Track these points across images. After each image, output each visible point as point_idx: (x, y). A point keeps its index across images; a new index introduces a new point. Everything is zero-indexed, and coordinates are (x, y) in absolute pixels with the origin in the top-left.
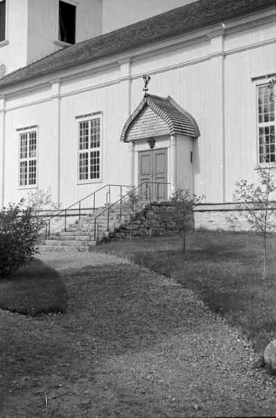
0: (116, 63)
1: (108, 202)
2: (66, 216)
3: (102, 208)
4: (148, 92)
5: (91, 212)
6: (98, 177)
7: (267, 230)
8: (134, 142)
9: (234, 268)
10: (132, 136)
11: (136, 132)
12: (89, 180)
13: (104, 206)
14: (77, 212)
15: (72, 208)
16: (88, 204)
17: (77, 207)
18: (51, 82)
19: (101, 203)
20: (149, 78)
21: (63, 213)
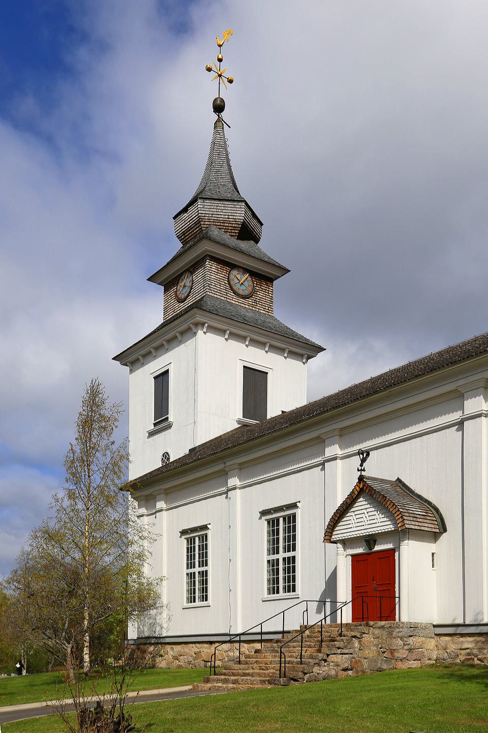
0: (318, 437)
1: (306, 624)
2: (240, 641)
3: (296, 631)
4: (363, 473)
5: (279, 636)
6: (294, 591)
7: (331, 685)
8: (345, 543)
9: (304, 361)
10: (338, 534)
11: (343, 531)
12: (282, 594)
13: (16, 558)
14: (258, 637)
15: (250, 631)
16: (274, 626)
17: (258, 630)
18: (227, 469)
19: (293, 625)
20: (368, 454)
21: (237, 638)
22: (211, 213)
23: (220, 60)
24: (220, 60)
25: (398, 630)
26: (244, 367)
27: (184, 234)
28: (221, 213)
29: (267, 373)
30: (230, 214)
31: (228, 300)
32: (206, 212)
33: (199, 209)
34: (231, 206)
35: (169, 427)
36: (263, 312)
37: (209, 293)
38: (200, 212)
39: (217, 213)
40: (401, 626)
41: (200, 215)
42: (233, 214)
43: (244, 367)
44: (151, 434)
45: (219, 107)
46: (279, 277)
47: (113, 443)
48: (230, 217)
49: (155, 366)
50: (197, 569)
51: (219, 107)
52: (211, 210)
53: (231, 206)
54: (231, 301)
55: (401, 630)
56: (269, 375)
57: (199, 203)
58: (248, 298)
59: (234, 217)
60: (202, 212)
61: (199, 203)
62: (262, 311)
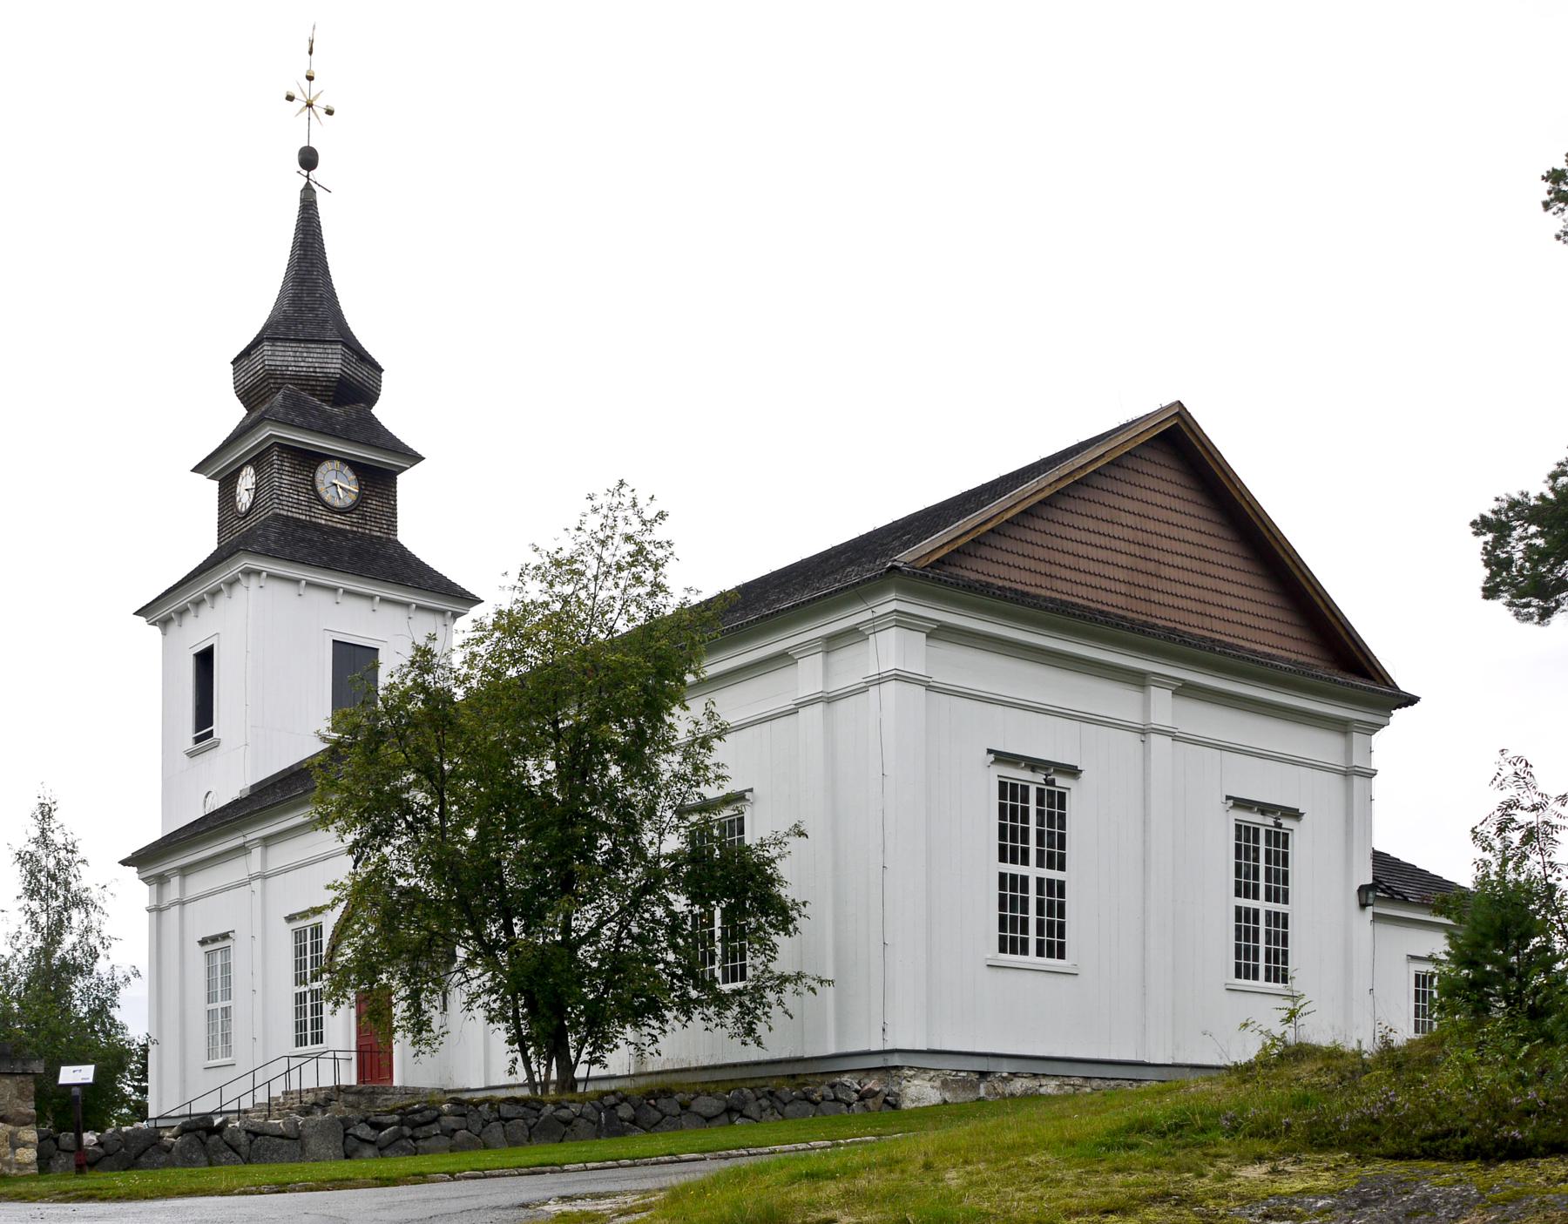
22: (286, 363)
23: (310, 78)
24: (310, 78)
25: (386, 1097)
26: (334, 641)
27: (247, 394)
28: (302, 364)
29: (377, 650)
30: (317, 365)
31: (314, 520)
32: (278, 363)
33: (265, 353)
34: (318, 350)
35: (216, 745)
36: (379, 534)
37: (278, 511)
38: (266, 363)
39: (297, 364)
40: (392, 1090)
41: (267, 367)
42: (324, 365)
43: (334, 641)
44: (192, 754)
45: (308, 159)
46: (407, 469)
47: (53, 832)
48: (318, 370)
49: (196, 632)
50: (220, 1005)
51: (308, 159)
52: (286, 358)
53: (318, 350)
54: (319, 521)
55: (390, 1096)
56: (380, 652)
57: (265, 348)
58: (349, 512)
59: (325, 370)
60: (270, 363)
61: (265, 348)
62: (375, 533)
